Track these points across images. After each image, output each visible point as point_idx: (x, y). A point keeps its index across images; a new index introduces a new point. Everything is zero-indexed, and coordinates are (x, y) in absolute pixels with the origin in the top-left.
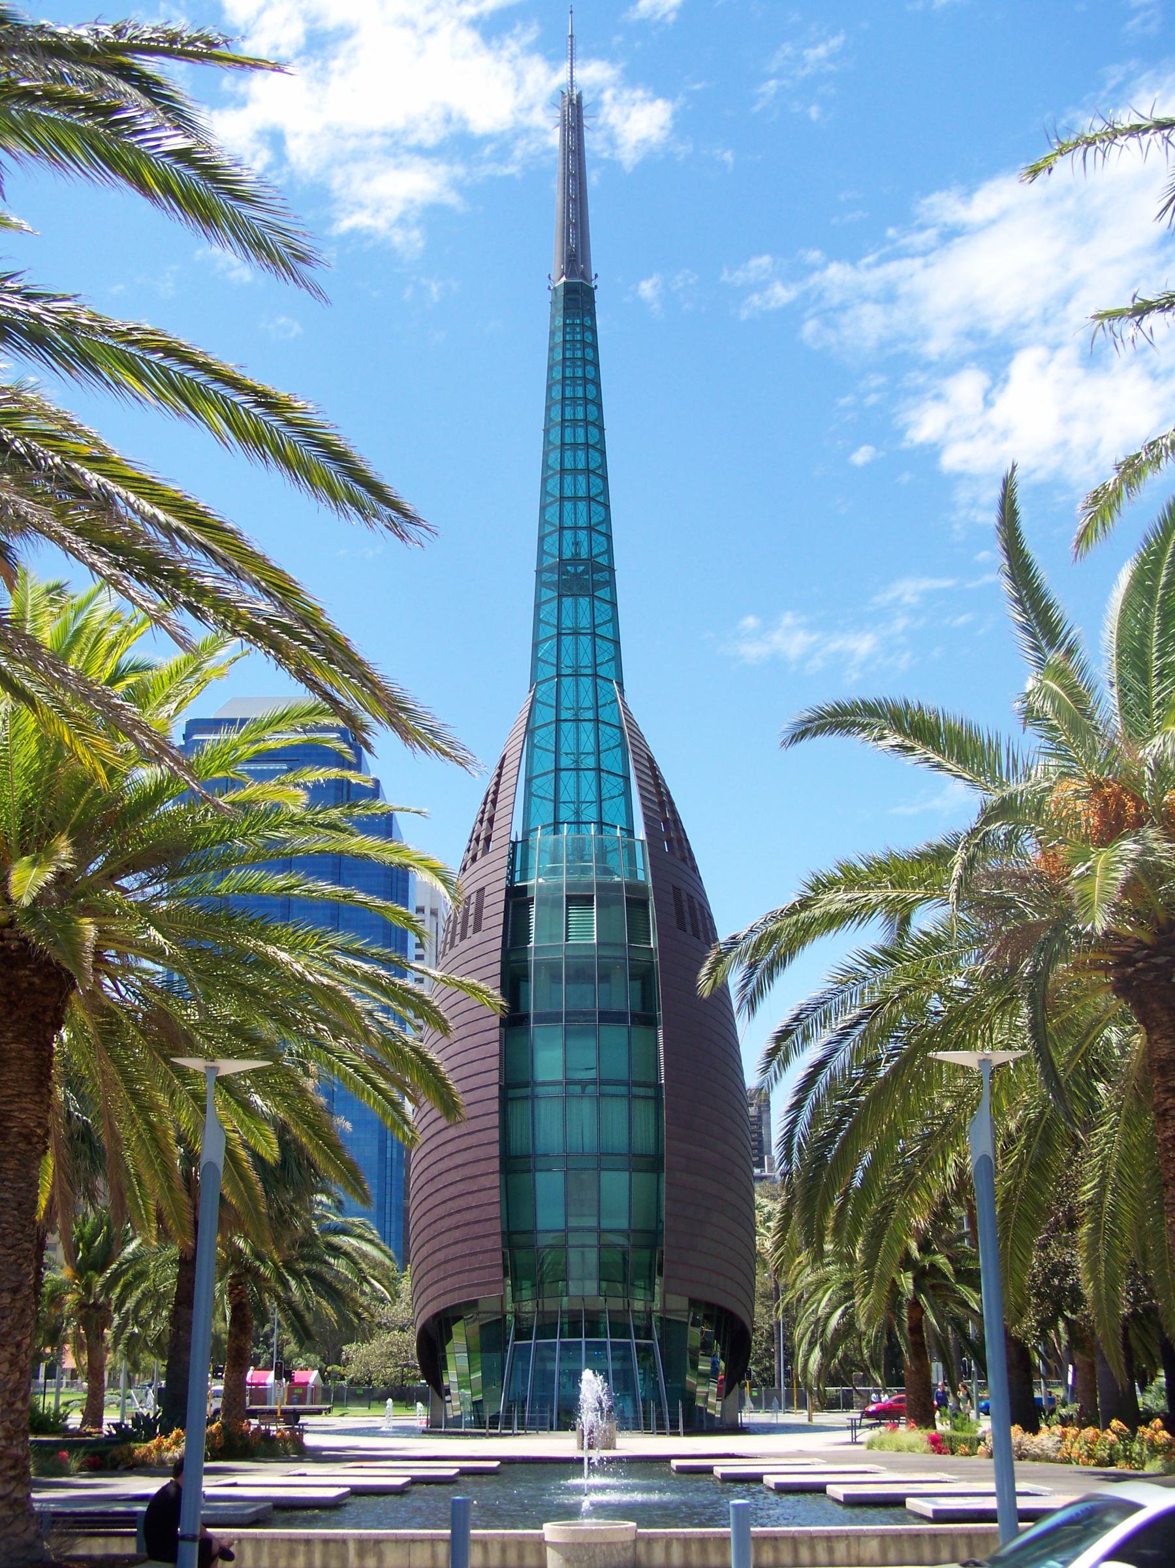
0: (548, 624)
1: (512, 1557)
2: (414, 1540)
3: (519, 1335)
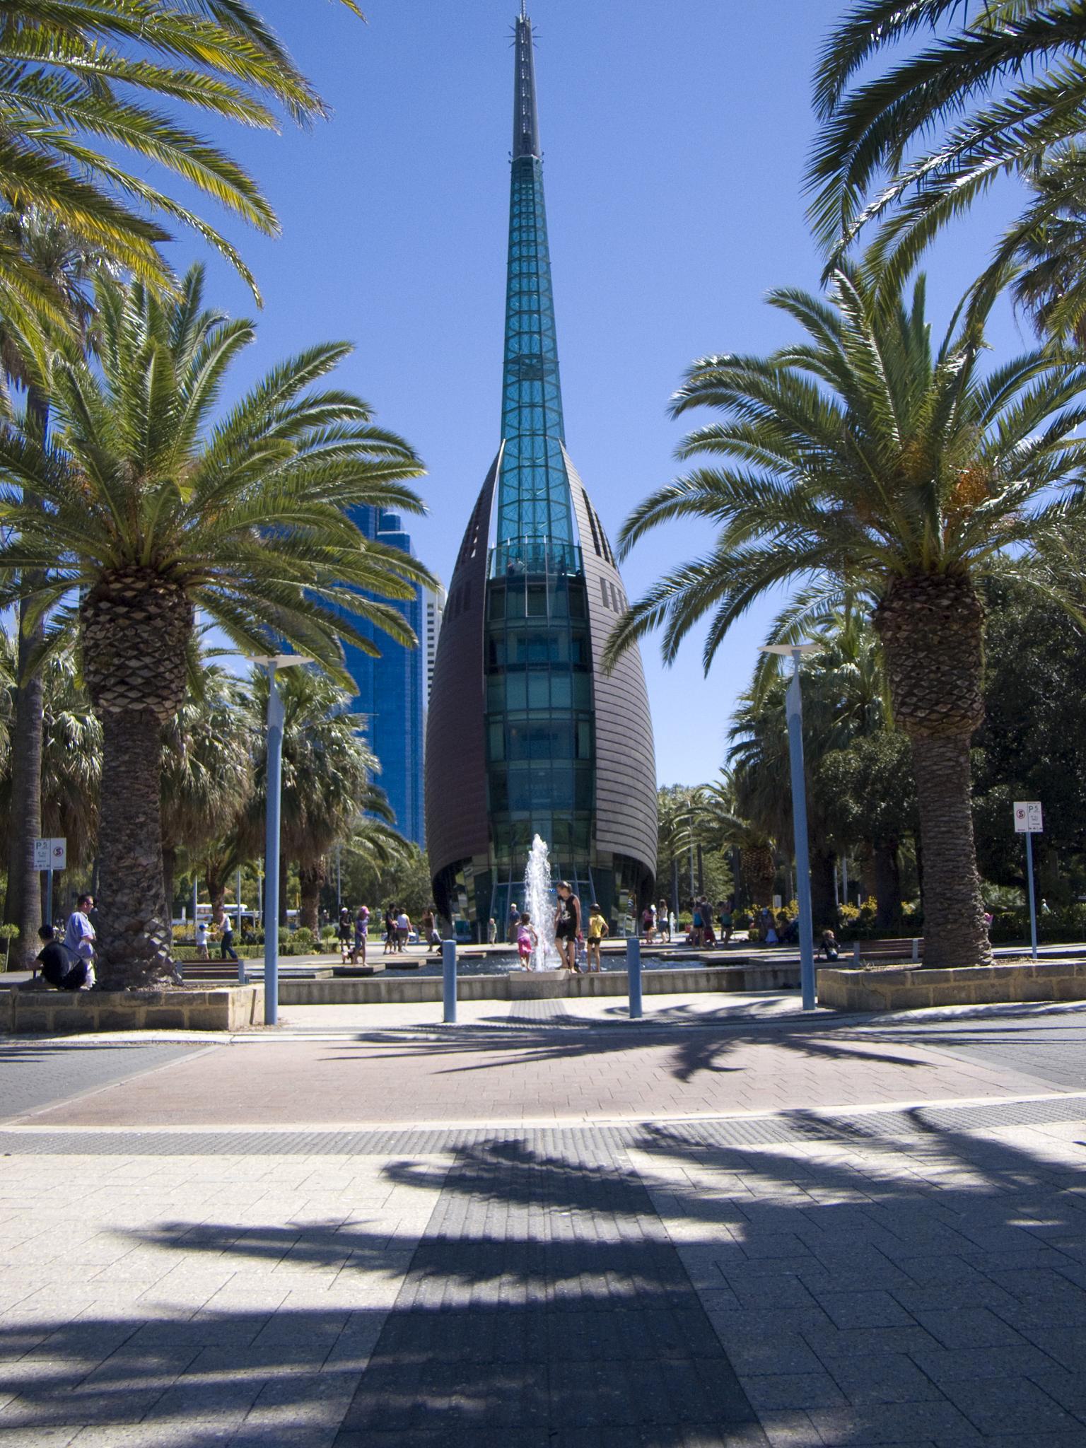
0: (512, 427)
2: (422, 983)
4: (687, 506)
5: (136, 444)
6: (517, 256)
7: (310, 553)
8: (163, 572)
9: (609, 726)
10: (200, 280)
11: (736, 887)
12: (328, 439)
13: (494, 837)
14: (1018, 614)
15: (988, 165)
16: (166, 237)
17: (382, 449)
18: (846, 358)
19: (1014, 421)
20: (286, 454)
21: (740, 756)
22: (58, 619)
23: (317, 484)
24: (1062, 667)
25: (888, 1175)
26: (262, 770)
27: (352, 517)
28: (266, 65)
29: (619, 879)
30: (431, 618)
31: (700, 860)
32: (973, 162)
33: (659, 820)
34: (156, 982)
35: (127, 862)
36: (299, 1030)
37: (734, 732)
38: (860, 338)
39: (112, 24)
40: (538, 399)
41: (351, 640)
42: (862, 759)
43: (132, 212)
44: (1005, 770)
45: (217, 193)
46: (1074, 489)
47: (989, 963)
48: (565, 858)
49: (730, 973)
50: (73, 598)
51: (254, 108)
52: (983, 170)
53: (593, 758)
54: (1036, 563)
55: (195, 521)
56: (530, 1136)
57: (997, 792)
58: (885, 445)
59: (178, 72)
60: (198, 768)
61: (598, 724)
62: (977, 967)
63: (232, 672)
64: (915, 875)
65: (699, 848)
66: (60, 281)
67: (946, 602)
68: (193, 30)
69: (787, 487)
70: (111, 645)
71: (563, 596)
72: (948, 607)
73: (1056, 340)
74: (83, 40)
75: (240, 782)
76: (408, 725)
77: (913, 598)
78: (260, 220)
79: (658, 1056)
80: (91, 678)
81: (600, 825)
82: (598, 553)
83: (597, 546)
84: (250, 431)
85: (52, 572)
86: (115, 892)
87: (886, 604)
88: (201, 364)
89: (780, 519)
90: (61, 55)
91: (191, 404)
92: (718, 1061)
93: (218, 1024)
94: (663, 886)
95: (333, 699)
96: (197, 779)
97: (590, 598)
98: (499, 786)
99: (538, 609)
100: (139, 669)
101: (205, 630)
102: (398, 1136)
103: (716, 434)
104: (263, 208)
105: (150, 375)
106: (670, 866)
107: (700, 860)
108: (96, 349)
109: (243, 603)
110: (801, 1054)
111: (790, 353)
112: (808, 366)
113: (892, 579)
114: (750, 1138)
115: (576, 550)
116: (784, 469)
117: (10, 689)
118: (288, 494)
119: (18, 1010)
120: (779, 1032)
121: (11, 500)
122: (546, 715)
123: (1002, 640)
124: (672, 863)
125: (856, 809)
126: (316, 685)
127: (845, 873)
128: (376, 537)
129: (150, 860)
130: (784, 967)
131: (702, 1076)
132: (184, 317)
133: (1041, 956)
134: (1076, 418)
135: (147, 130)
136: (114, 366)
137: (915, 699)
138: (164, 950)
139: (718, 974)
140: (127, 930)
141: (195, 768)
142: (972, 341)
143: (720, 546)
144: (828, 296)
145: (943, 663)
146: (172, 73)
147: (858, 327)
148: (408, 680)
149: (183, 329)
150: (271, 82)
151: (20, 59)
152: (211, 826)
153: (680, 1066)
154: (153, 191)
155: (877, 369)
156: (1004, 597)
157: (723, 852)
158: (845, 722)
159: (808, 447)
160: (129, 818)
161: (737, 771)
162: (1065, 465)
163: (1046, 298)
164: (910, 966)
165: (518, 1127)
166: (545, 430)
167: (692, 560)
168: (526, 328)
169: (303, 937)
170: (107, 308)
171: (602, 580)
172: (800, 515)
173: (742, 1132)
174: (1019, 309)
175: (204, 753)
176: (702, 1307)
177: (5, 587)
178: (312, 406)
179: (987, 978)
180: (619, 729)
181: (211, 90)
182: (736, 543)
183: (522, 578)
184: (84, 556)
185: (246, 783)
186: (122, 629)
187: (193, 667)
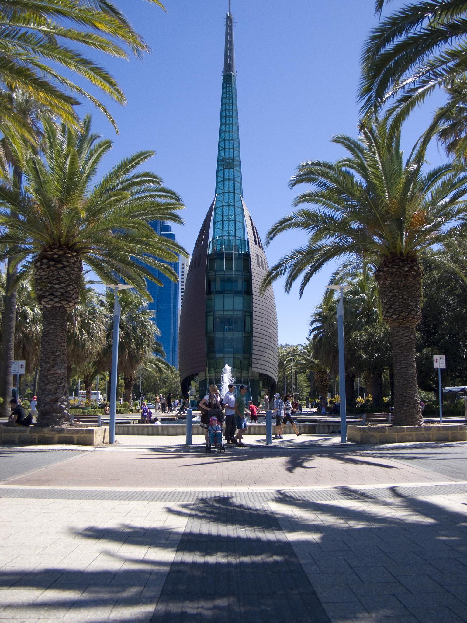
1: (183, 294)
4: (296, 225)
5: (60, 192)
6: (224, 115)
7: (133, 240)
8: (70, 247)
9: (258, 318)
10: (89, 122)
11: (311, 389)
12: (143, 192)
13: (208, 365)
14: (436, 274)
15: (431, 84)
16: (78, 103)
17: (166, 196)
18: (366, 163)
19: (437, 192)
20: (125, 198)
21: (315, 333)
22: (24, 266)
23: (137, 211)
24: (454, 298)
25: (381, 516)
26: (110, 333)
27: (152, 226)
28: (124, 30)
29: (261, 384)
30: (183, 270)
31: (296, 377)
32: (424, 82)
33: (279, 359)
34: (63, 424)
35: (52, 372)
36: (124, 446)
37: (313, 322)
38: (372, 154)
39: (58, 12)
40: (232, 177)
41: (150, 279)
42: (368, 335)
43: (64, 92)
44: (430, 341)
45: (100, 86)
46: (460, 221)
47: (421, 425)
48: (239, 375)
49: (309, 426)
50: (30, 258)
51: (118, 50)
52: (429, 85)
53: (251, 332)
54: (444, 253)
55: (85, 226)
56: (234, 495)
57: (425, 351)
58: (382, 201)
59: (86, 33)
60: (82, 331)
61: (254, 317)
62: (417, 426)
63: (96, 291)
64: (389, 385)
65: (296, 371)
66: (29, 121)
67: (406, 269)
68: (93, 15)
69: (340, 218)
70: (47, 278)
71: (240, 262)
72: (407, 271)
73: (458, 158)
74: (45, 19)
75: (100, 338)
76: (172, 316)
77: (393, 267)
78: (118, 98)
79: (279, 462)
80: (38, 292)
81: (253, 360)
82: (256, 244)
83: (255, 241)
84: (110, 188)
85: (23, 246)
86: (46, 385)
87: (381, 269)
88: (89, 159)
89: (336, 231)
90: (36, 25)
91: (85, 176)
92: (306, 464)
93: (90, 443)
94: (280, 387)
95: (141, 304)
96: (82, 337)
97: (252, 263)
98: (211, 343)
99: (230, 267)
100: (59, 289)
101: (86, 272)
102: (168, 493)
103: (310, 195)
104: (119, 93)
105: (68, 162)
106: (283, 379)
107: (296, 377)
108: (44, 150)
109: (104, 262)
110: (342, 462)
111: (342, 161)
112: (350, 167)
113: (384, 258)
114: (321, 498)
115: (246, 242)
116: (339, 210)
117: (2, 296)
118: (126, 216)
119: (3, 434)
120: (332, 452)
121: (6, 215)
122: (232, 313)
123: (429, 285)
124: (284, 378)
125: (365, 357)
126: (134, 297)
127: (358, 384)
128: (160, 234)
129: (61, 371)
130: (332, 424)
131: (299, 470)
132: (83, 139)
133: (444, 422)
134: (464, 192)
135: (71, 58)
136: (51, 158)
137: (392, 310)
138: (67, 410)
139: (304, 426)
140: (51, 401)
141: (81, 332)
142: (419, 159)
143: (310, 242)
144: (359, 137)
145: (405, 295)
146: (83, 34)
147: (371, 149)
148: (172, 296)
149: (82, 142)
150: (125, 37)
151: (19, 26)
152: (87, 357)
153: (289, 466)
154: (72, 83)
155: (379, 168)
156: (430, 266)
157: (306, 374)
158: (360, 319)
159: (349, 201)
160: (53, 353)
161: (314, 339)
162: (458, 212)
163: (452, 139)
164: (387, 425)
165: (204, 490)
166: (234, 190)
167: (298, 248)
168: (227, 147)
169: (125, 406)
170: (48, 132)
171: (257, 255)
172: (345, 230)
173: (317, 495)
174: (440, 144)
175: (84, 325)
176: (304, 572)
177: (2, 252)
178: (136, 178)
179: (421, 431)
180: (263, 320)
181: (100, 41)
182: (317, 241)
183: (223, 254)
184: (36, 239)
185: (102, 339)
186: (52, 271)
187: (82, 288)
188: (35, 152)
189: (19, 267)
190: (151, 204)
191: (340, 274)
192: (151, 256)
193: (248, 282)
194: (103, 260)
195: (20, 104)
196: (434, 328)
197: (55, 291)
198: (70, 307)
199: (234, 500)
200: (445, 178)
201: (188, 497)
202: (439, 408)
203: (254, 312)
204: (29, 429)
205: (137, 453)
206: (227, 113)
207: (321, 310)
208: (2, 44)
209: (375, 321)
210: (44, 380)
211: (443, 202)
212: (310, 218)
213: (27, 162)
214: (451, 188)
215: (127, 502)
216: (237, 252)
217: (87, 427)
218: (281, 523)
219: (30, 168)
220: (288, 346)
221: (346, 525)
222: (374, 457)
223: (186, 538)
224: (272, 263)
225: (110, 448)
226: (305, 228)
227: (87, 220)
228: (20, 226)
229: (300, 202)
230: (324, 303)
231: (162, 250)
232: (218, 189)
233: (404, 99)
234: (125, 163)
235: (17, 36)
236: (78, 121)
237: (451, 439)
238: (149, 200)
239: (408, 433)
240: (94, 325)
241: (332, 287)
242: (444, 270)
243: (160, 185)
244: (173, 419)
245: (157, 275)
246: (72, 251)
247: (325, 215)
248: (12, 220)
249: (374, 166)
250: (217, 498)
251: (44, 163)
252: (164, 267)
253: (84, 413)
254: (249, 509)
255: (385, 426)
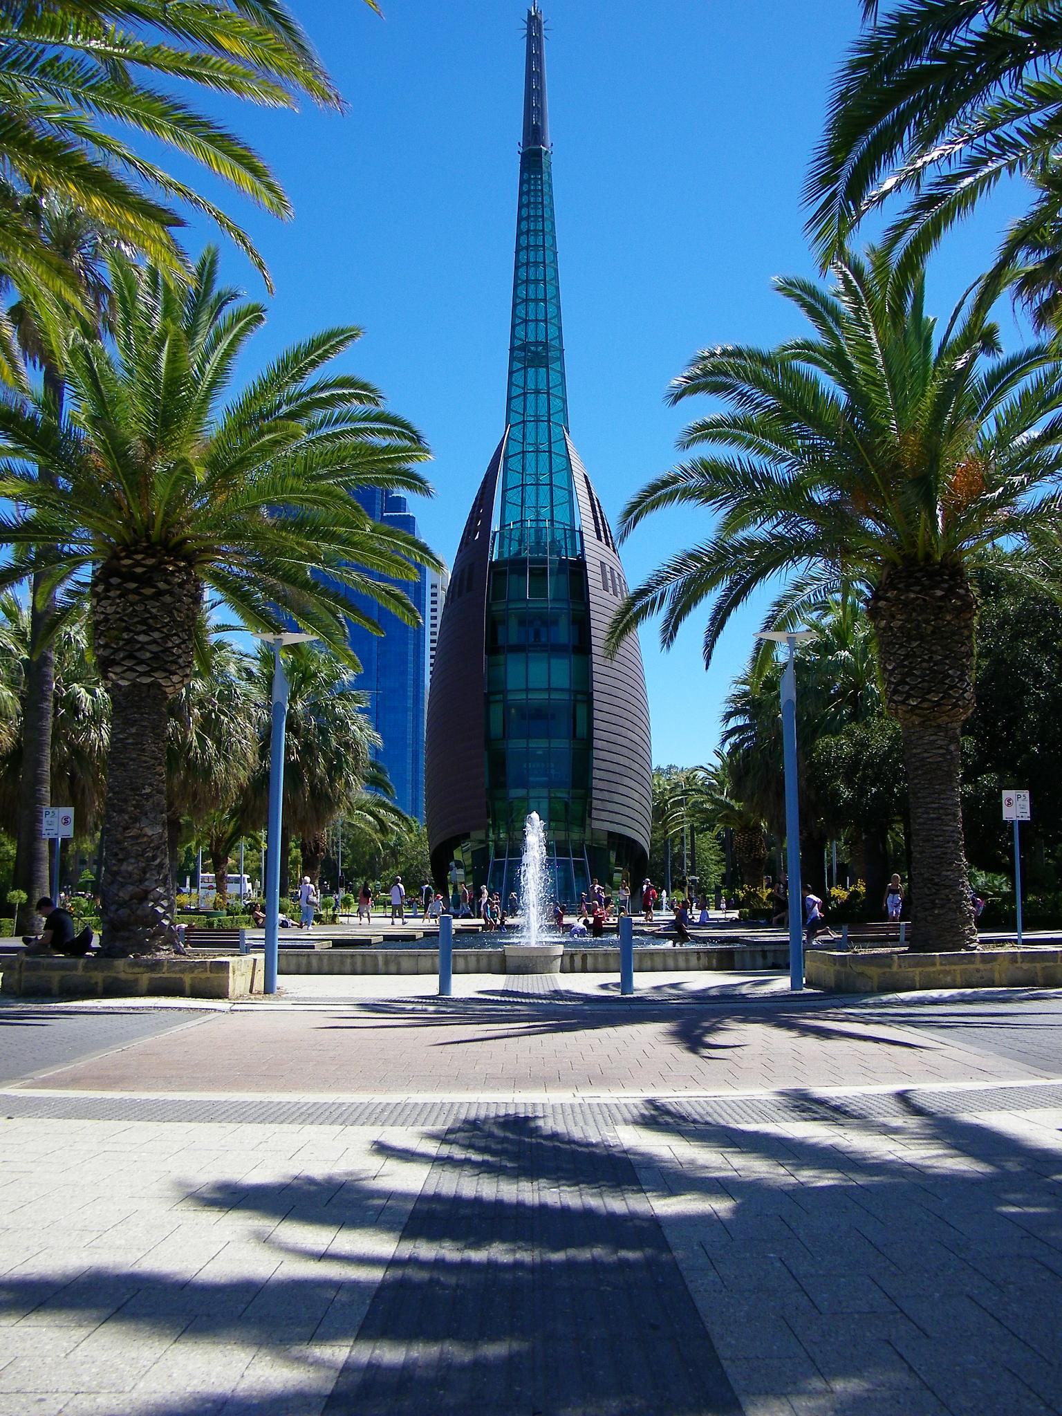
3: (497, 855)
4: (688, 494)
7: (315, 532)
9: (606, 707)
10: (214, 262)
11: (727, 867)
12: (337, 421)
14: (1010, 605)
15: (993, 166)
16: (180, 223)
17: (389, 433)
19: (1010, 415)
20: (295, 436)
22: (70, 593)
24: (1052, 658)
27: (359, 499)
30: (434, 599)
32: (975, 164)
34: (159, 950)
36: (297, 999)
37: (728, 716)
40: (542, 386)
41: (355, 618)
42: (854, 745)
43: (145, 197)
45: (230, 176)
47: (975, 948)
48: (561, 836)
49: (721, 951)
50: (85, 573)
52: (987, 170)
53: (590, 738)
54: (1031, 557)
57: (986, 780)
59: (195, 54)
61: (596, 705)
62: (963, 952)
65: (692, 827)
67: (939, 593)
70: (121, 620)
71: (564, 579)
72: (941, 598)
76: (410, 703)
77: (908, 589)
78: (272, 203)
80: (101, 652)
81: (595, 803)
82: (599, 538)
83: (598, 531)
86: (121, 861)
87: (880, 593)
88: (213, 347)
89: (780, 509)
90: (80, 37)
91: (203, 385)
93: (219, 993)
94: (656, 864)
95: (338, 677)
96: (204, 752)
97: (590, 582)
98: (498, 763)
99: (539, 590)
100: (148, 643)
101: (213, 606)
103: (718, 424)
105: (164, 356)
109: (251, 581)
111: (792, 347)
112: (810, 360)
114: (737, 1117)
116: (784, 459)
117: (22, 660)
120: (772, 1012)
123: (993, 630)
124: (666, 842)
125: (847, 794)
127: (834, 855)
129: (154, 831)
132: (198, 301)
133: (1026, 942)
135: (163, 115)
137: (907, 687)
138: (167, 918)
145: (936, 652)
146: (188, 56)
148: (411, 658)
149: (196, 309)
151: (40, 42)
154: (167, 176)
160: (136, 789)
164: (897, 949)
167: (690, 547)
170: (121, 288)
173: (729, 1111)
174: (1018, 305)
175: (210, 726)
176: (686, 1287)
179: (973, 963)
182: (736, 531)
184: (97, 532)
185: (250, 756)
186: (132, 605)
187: (202, 642)
188: (89, 332)
189: (59, 593)
190: (354, 449)
191: (789, 606)
192: (357, 568)
193: (582, 623)
194: (248, 578)
195: (58, 222)
196: (1004, 728)
197: (139, 650)
198: (174, 685)
199: (540, 1123)
200: (1027, 382)
201: (434, 1115)
202: (1015, 911)
203: (595, 694)
204: (82, 961)
205: (326, 1014)
206: (532, 239)
207: (748, 687)
208: (4, 84)
209: (870, 711)
210: (112, 851)
211: (1022, 439)
212: (717, 479)
213: (72, 354)
214: (1040, 408)
215: (295, 1127)
216: (555, 557)
217: (215, 957)
218: (642, 1174)
219: (78, 369)
220: (673, 771)
221: (792, 1180)
222: (867, 1023)
223: (425, 1207)
224: (634, 583)
225: (267, 1003)
226: (706, 501)
227: (210, 484)
228: (59, 502)
229: (694, 439)
230: (753, 670)
231: (381, 554)
232: (512, 414)
233: (927, 203)
234: (296, 356)
235: (38, 66)
236: (183, 260)
237: (1041, 980)
238: (350, 440)
239: (943, 968)
240: (232, 725)
241: (770, 635)
242: (1029, 594)
243: (377, 405)
244: (412, 938)
245: (376, 613)
246: (176, 559)
247: (754, 471)
248: (39, 488)
249: (866, 356)
250: (501, 1120)
251: (110, 358)
252: (387, 592)
253: (211, 924)
254: (572, 1141)
255: (893, 953)
